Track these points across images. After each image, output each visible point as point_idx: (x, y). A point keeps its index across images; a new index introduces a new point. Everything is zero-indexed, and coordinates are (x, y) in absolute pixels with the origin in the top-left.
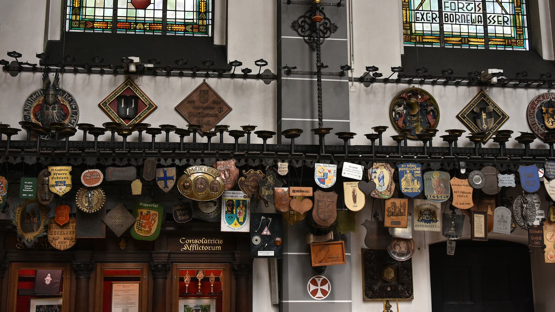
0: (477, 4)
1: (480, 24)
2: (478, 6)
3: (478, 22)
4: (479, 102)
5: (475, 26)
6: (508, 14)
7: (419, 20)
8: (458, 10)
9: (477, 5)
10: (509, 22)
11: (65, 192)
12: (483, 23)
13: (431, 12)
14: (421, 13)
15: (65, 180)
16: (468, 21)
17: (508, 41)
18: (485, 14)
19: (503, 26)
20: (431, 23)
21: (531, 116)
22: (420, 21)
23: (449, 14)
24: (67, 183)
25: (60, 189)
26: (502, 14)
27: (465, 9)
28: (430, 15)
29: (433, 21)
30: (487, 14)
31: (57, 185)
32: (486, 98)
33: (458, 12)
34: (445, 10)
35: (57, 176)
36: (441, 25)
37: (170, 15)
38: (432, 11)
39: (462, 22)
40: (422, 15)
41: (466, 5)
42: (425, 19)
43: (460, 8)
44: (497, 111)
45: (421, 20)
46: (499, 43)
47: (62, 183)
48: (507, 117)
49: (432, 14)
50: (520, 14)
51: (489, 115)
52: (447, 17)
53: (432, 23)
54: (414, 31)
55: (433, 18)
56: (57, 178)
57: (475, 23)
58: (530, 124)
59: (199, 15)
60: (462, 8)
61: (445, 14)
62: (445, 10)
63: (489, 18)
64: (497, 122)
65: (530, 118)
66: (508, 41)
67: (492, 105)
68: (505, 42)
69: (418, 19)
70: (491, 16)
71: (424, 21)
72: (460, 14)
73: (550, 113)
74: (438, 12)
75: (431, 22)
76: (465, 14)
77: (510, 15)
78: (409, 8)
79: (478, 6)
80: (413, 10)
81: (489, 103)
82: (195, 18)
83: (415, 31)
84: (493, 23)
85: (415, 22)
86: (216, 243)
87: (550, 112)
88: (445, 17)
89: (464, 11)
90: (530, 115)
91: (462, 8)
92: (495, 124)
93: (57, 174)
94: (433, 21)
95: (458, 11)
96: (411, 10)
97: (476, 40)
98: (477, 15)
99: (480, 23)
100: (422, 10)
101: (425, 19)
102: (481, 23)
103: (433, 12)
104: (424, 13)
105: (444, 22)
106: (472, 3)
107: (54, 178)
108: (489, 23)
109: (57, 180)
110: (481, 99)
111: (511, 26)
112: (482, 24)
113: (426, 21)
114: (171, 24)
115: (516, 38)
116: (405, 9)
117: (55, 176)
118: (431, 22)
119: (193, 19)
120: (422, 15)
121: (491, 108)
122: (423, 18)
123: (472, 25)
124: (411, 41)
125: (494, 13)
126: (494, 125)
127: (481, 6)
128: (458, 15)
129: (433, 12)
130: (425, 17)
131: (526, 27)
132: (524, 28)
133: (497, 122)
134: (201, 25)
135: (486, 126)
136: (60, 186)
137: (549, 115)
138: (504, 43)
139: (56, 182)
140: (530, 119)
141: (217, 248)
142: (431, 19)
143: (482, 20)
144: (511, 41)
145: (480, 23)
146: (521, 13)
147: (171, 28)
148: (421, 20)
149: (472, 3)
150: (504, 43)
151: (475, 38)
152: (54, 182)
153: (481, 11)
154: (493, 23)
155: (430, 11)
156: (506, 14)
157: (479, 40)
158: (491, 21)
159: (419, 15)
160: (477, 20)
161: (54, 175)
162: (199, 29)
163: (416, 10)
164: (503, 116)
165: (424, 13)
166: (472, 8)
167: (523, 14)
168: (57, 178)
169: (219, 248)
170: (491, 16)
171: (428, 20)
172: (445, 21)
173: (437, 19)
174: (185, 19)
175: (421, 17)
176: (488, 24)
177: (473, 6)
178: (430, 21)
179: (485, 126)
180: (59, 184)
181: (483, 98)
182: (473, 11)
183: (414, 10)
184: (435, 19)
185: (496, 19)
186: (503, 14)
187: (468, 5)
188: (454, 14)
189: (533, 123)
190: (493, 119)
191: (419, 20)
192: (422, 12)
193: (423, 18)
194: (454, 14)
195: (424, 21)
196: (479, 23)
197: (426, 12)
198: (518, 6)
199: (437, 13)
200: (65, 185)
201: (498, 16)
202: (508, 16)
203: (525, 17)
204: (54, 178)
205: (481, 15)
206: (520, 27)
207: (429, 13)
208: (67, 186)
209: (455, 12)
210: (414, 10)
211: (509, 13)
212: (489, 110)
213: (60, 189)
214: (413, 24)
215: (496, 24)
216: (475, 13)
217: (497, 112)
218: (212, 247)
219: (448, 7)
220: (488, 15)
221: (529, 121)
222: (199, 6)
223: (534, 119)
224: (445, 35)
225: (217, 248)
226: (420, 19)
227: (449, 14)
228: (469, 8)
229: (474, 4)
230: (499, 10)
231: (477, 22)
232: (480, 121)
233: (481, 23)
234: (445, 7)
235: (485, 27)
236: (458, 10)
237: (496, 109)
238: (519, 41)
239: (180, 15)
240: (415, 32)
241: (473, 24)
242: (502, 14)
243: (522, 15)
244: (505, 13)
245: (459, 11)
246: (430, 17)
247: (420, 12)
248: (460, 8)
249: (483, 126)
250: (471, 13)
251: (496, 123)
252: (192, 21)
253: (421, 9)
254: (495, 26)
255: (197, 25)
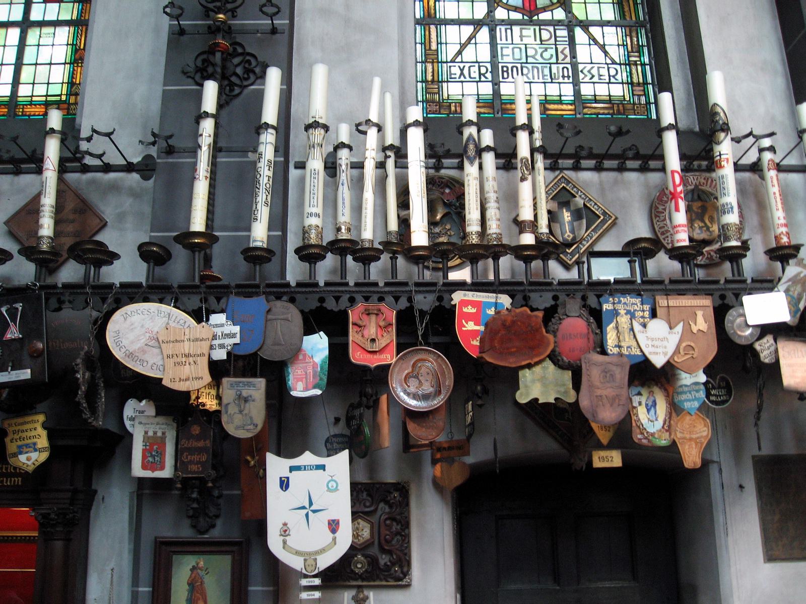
0: (560, 48)
1: (566, 80)
2: (562, 52)
3: (563, 77)
4: (555, 192)
5: (558, 84)
6: (616, 64)
7: (455, 78)
8: (527, 60)
9: (559, 50)
10: (619, 77)
11: (37, 464)
12: (571, 79)
13: (477, 65)
14: (459, 67)
15: (35, 440)
16: (545, 77)
17: (618, 107)
18: (574, 65)
19: (608, 83)
20: (477, 82)
21: (659, 217)
22: (457, 80)
23: (510, 66)
24: (39, 446)
25: (28, 459)
26: (606, 63)
27: (538, 57)
28: (476, 69)
29: (480, 78)
30: (579, 65)
31: (21, 453)
32: (571, 184)
33: (527, 63)
34: (502, 59)
35: (19, 436)
36: (496, 84)
37: (24, 91)
38: (479, 63)
39: (533, 79)
40: (462, 70)
41: (540, 51)
42: (467, 75)
43: (530, 57)
44: (593, 207)
45: (459, 78)
46: (601, 111)
47: (30, 447)
48: (614, 218)
49: (479, 67)
50: (638, 63)
51: (577, 215)
52: (507, 71)
53: (480, 81)
54: (446, 96)
55: (480, 74)
56: (20, 438)
57: (558, 79)
58: (657, 231)
59: (72, 87)
60: (533, 57)
61: (503, 67)
62: (502, 59)
63: (582, 71)
64: (593, 228)
65: (658, 221)
66: (618, 107)
67: (583, 196)
68: (612, 108)
69: (453, 76)
70: (585, 68)
71: (465, 78)
72: (530, 66)
73: (696, 210)
74: (490, 64)
75: (478, 79)
76: (539, 66)
77: (620, 64)
78: (438, 58)
79: (562, 52)
80: (444, 62)
81: (577, 193)
82: (64, 92)
83: (448, 95)
84: (591, 79)
85: (448, 82)
86: (12, 470)
87: (695, 208)
88: (503, 71)
89: (537, 60)
90: (656, 216)
91: (533, 57)
92: (587, 234)
93: (18, 431)
94: (480, 78)
95: (525, 61)
96: (442, 62)
97: (560, 107)
98: (561, 66)
99: (566, 79)
100: (462, 62)
101: (467, 75)
102: (569, 79)
103: (481, 64)
104: (464, 67)
105: (501, 79)
106: (552, 48)
107: (14, 441)
108: (583, 79)
109: (19, 443)
110: (561, 186)
111: (622, 83)
112: (571, 80)
113: (468, 79)
114: (23, 105)
115: (632, 102)
116: (431, 60)
117: (16, 436)
118: (478, 79)
119: (60, 95)
120: (462, 70)
121: (579, 201)
122: (462, 74)
123: (552, 82)
124: (440, 111)
125: (592, 63)
126: (587, 234)
127: (567, 52)
128: (527, 67)
129: (481, 64)
130: (466, 72)
131: (650, 84)
132: (646, 86)
133: (593, 228)
134: (72, 104)
135: (572, 236)
136: (27, 453)
137: (693, 215)
138: (611, 111)
139: (19, 447)
140: (658, 223)
141: (15, 481)
142: (476, 75)
143: (570, 74)
144: (623, 106)
145: (566, 79)
146: (640, 61)
147: (22, 112)
148: (459, 78)
149: (552, 48)
150: (611, 111)
151: (557, 104)
152: (15, 447)
153: (568, 60)
154: (591, 79)
155: (477, 62)
156: (613, 64)
157: (564, 107)
158: (586, 76)
159: (456, 70)
160: (561, 74)
161: (14, 434)
162: (68, 109)
163: (451, 62)
164: (604, 216)
165: (464, 67)
166: (552, 56)
167: (643, 62)
168: (20, 438)
169: (18, 480)
170: (585, 68)
171: (472, 76)
172: (503, 78)
173: (489, 75)
174: (47, 96)
175: (459, 72)
176: (581, 81)
177: (553, 52)
178: (475, 78)
179: (569, 236)
180: (25, 450)
181: (565, 186)
182: (554, 60)
183: (447, 62)
184: (484, 75)
185: (595, 72)
186: (608, 64)
187: (544, 51)
188: (519, 66)
189: (663, 230)
190: (584, 221)
191: (455, 78)
192: (462, 65)
193: (462, 74)
194: (519, 66)
195: (465, 78)
196: (564, 79)
197: (467, 65)
198: (634, 50)
199: (489, 66)
200: (36, 450)
201: (599, 68)
202: (618, 67)
203: (648, 67)
204: (14, 441)
205: (569, 66)
206: (636, 65)
207: (474, 66)
208: (40, 450)
209: (521, 63)
210: (447, 62)
211: (618, 62)
212: (576, 205)
213: (28, 459)
214: (445, 85)
215: (596, 79)
216: (557, 63)
217: (593, 209)
218: (5, 479)
219: (508, 55)
220: (581, 67)
221: (656, 226)
222: (73, 73)
223: (665, 222)
224: (503, 101)
225: (15, 481)
226: (457, 76)
227: (510, 66)
228: (547, 55)
229: (554, 50)
230: (598, 56)
231: (561, 78)
232: (559, 226)
233: (569, 79)
234: (502, 55)
235: (576, 83)
236: (527, 60)
237: (591, 205)
238: (637, 107)
239: (40, 90)
240: (448, 97)
241: (553, 81)
242: (606, 63)
243: (641, 65)
244: (611, 62)
245: (528, 61)
246: (475, 72)
247: (457, 65)
248: (530, 57)
249: (566, 235)
250: (550, 64)
251: (590, 230)
252: (58, 98)
253: (459, 59)
254: (594, 83)
255: (66, 103)
